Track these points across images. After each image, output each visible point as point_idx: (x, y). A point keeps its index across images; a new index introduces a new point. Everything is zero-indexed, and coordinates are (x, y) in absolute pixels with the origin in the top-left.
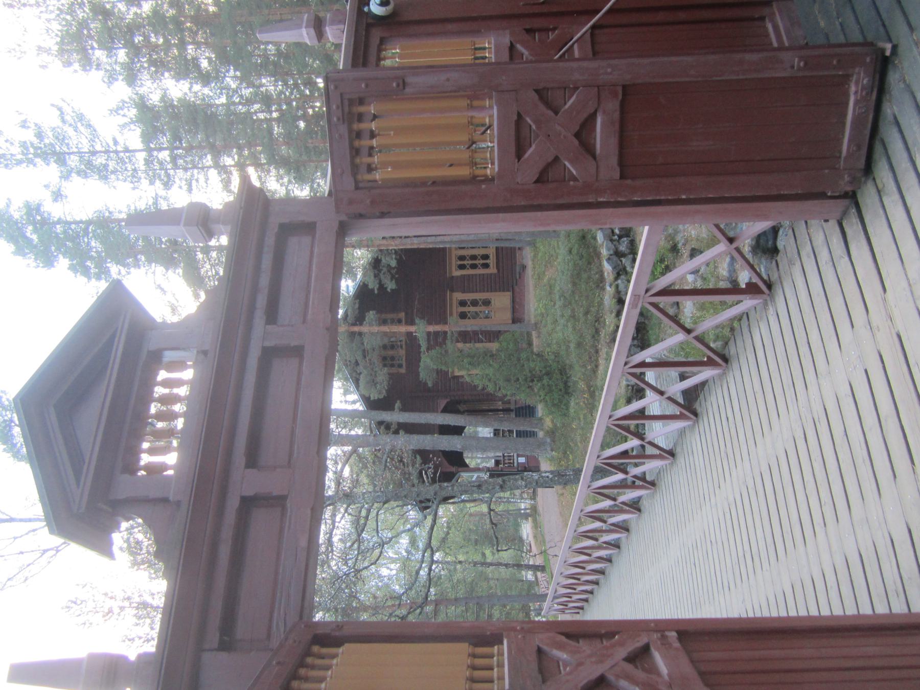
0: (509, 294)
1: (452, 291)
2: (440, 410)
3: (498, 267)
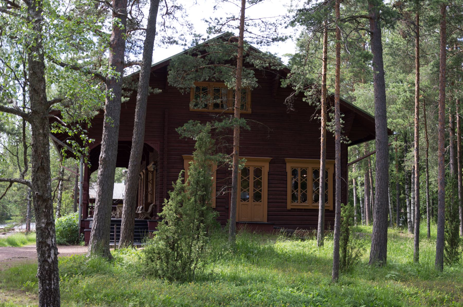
0: (265, 221)
1: (270, 163)
2: (146, 142)
3: (292, 210)
